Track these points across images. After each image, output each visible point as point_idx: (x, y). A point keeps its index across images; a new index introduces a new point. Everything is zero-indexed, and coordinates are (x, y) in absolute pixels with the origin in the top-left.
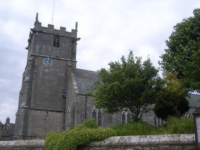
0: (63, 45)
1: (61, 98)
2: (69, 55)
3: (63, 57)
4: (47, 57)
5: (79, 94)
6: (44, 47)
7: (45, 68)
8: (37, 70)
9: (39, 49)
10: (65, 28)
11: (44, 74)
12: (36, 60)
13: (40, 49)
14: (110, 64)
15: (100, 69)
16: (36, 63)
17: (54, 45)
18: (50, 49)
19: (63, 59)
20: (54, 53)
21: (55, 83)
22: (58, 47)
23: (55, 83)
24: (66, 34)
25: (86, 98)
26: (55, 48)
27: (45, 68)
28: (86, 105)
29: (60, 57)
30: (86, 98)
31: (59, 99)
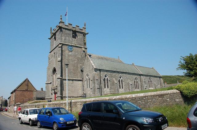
1: (80, 71)
3: (79, 45)
11: (69, 56)
13: (65, 39)
21: (76, 62)
23: (76, 62)
26: (74, 39)
31: (79, 72)
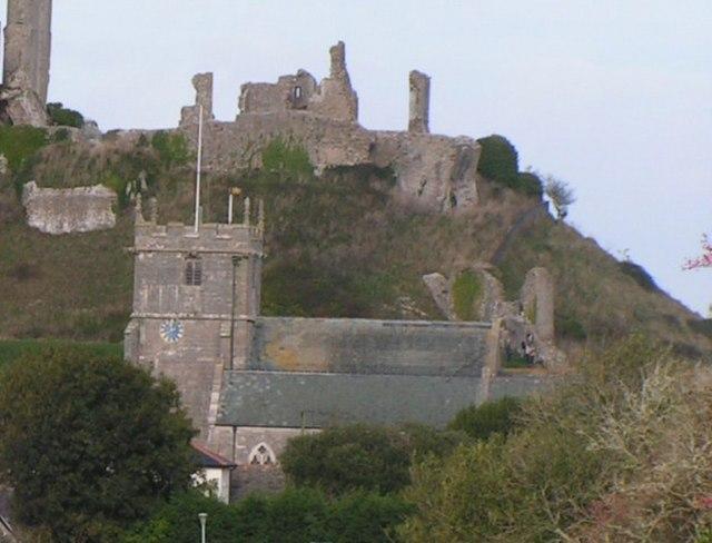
0: (212, 278)
2: (229, 302)
4: (169, 319)
5: (216, 425)
6: (161, 291)
7: (166, 347)
8: (146, 354)
9: (149, 297)
10: (60, 105)
12: (143, 329)
13: (153, 297)
14: (340, 42)
15: (478, 132)
16: (143, 337)
17: (189, 281)
18: (177, 296)
19: (211, 316)
20: (186, 304)
22: (198, 283)
24: (217, 245)
25: (235, 431)
26: (188, 289)
27: (166, 347)
28: (234, 446)
29: (204, 312)
30: (235, 431)
